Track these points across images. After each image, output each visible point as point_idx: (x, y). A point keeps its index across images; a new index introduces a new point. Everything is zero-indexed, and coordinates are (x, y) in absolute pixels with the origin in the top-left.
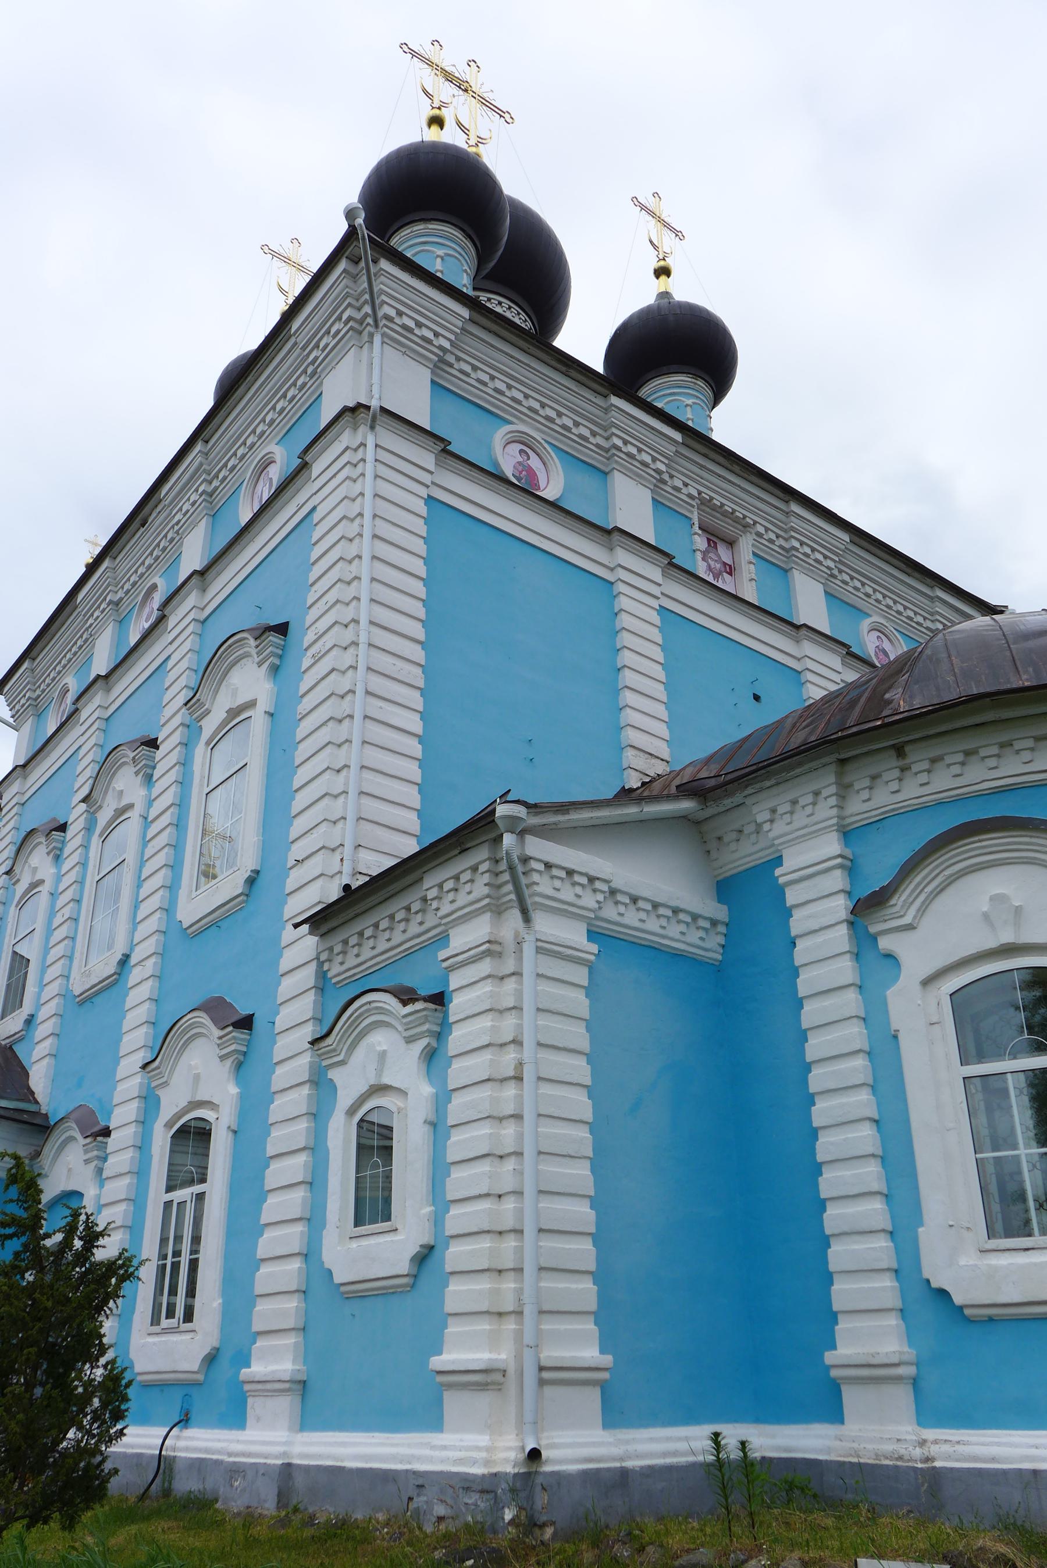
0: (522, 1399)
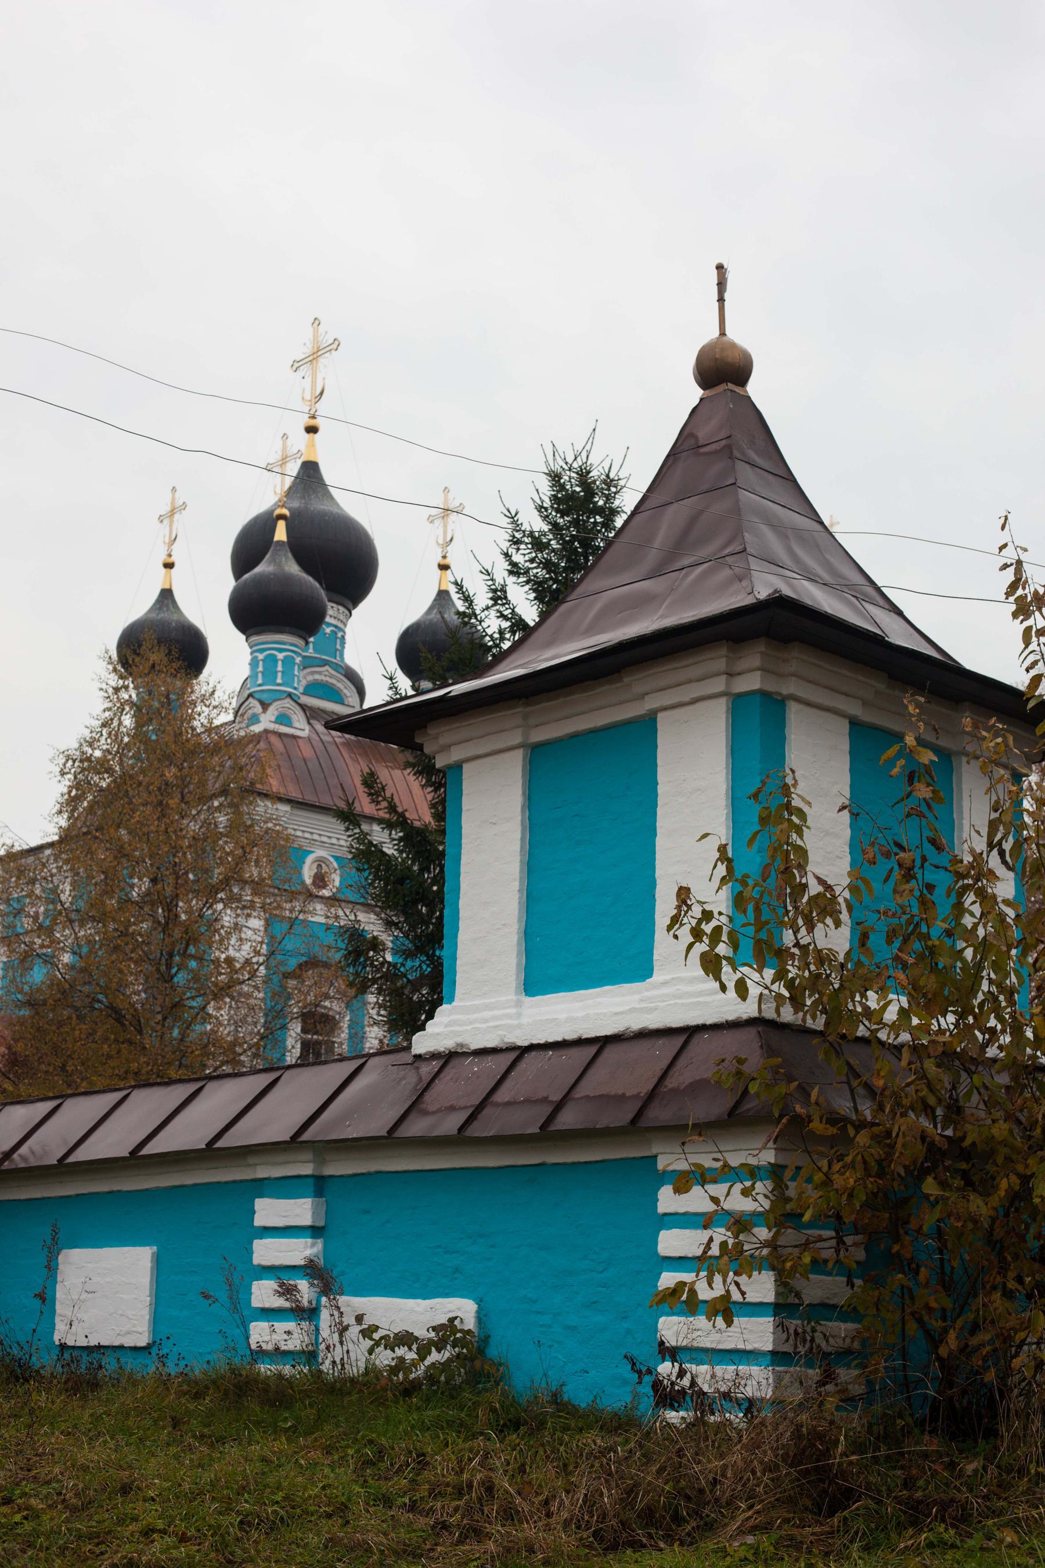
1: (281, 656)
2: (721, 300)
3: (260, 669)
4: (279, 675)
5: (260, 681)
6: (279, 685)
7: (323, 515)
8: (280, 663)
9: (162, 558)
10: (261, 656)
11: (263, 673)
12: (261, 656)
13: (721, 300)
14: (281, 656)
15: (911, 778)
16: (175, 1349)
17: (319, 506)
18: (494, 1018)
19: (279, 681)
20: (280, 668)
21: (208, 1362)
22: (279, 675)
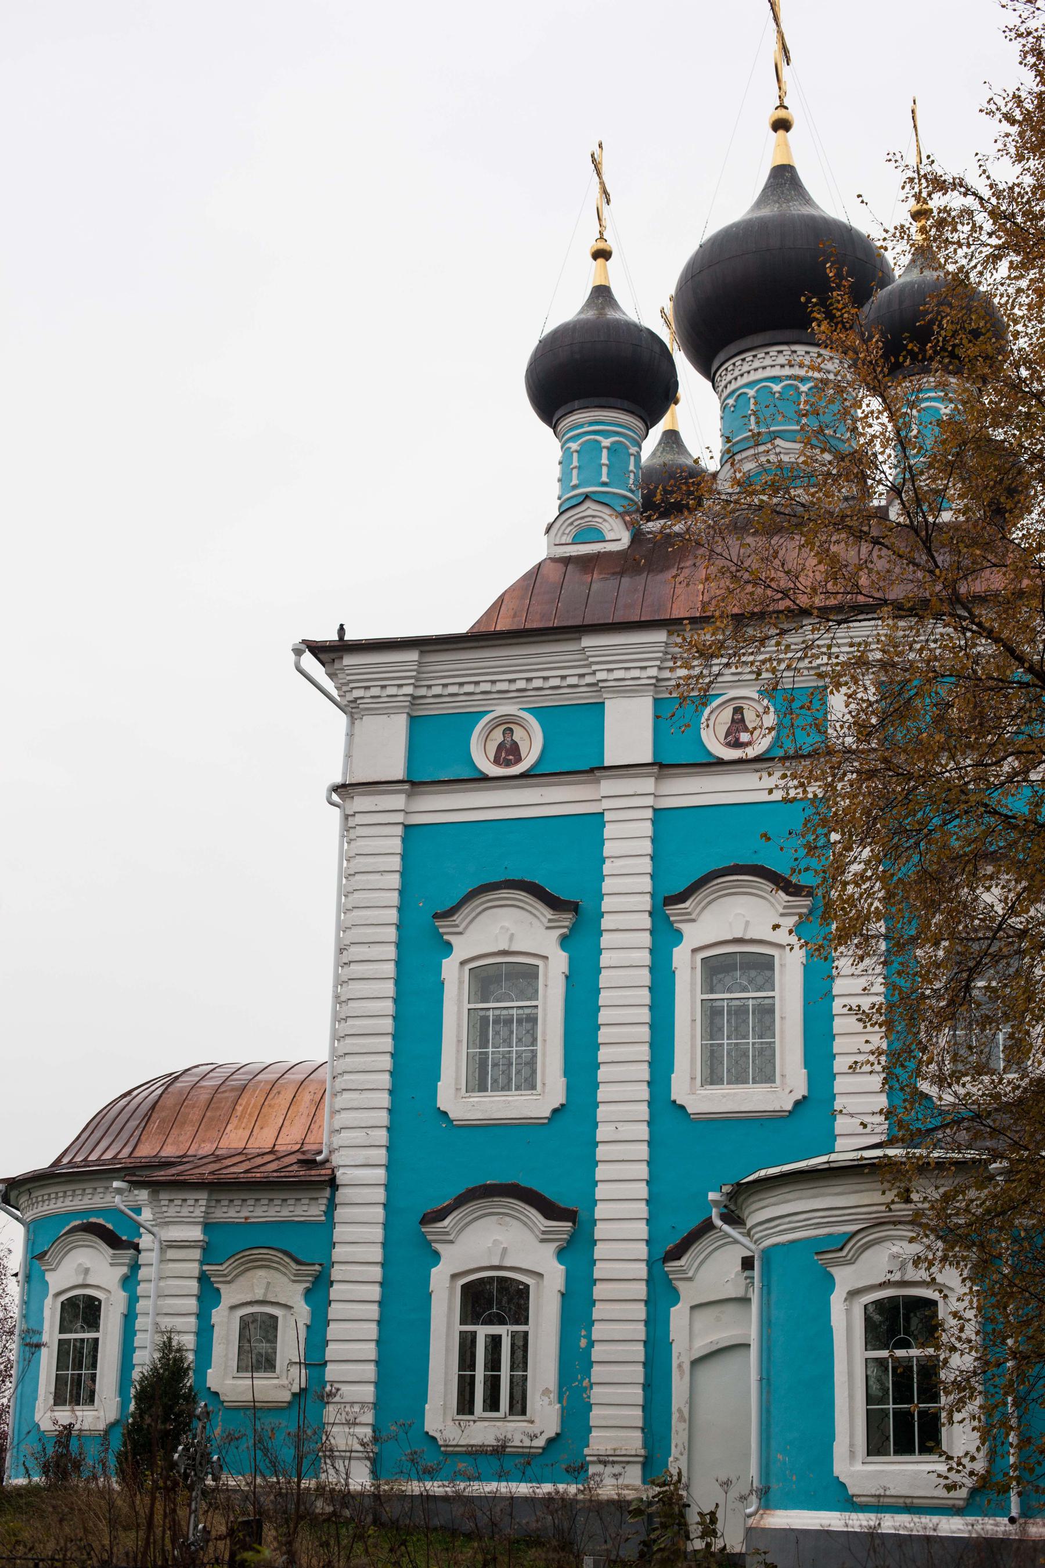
0: (847, 1326)
1: (606, 442)
2: (776, 19)
3: (575, 463)
4: (605, 470)
5: (575, 482)
6: (605, 484)
7: (618, 321)
8: (605, 452)
9: (770, 114)
10: (574, 446)
11: (579, 468)
12: (574, 446)
13: (776, 19)
14: (606, 442)
15: (958, 569)
16: (787, 844)
17: (612, 314)
18: (869, 620)
19: (604, 479)
20: (604, 460)
21: (808, 735)
22: (605, 470)
